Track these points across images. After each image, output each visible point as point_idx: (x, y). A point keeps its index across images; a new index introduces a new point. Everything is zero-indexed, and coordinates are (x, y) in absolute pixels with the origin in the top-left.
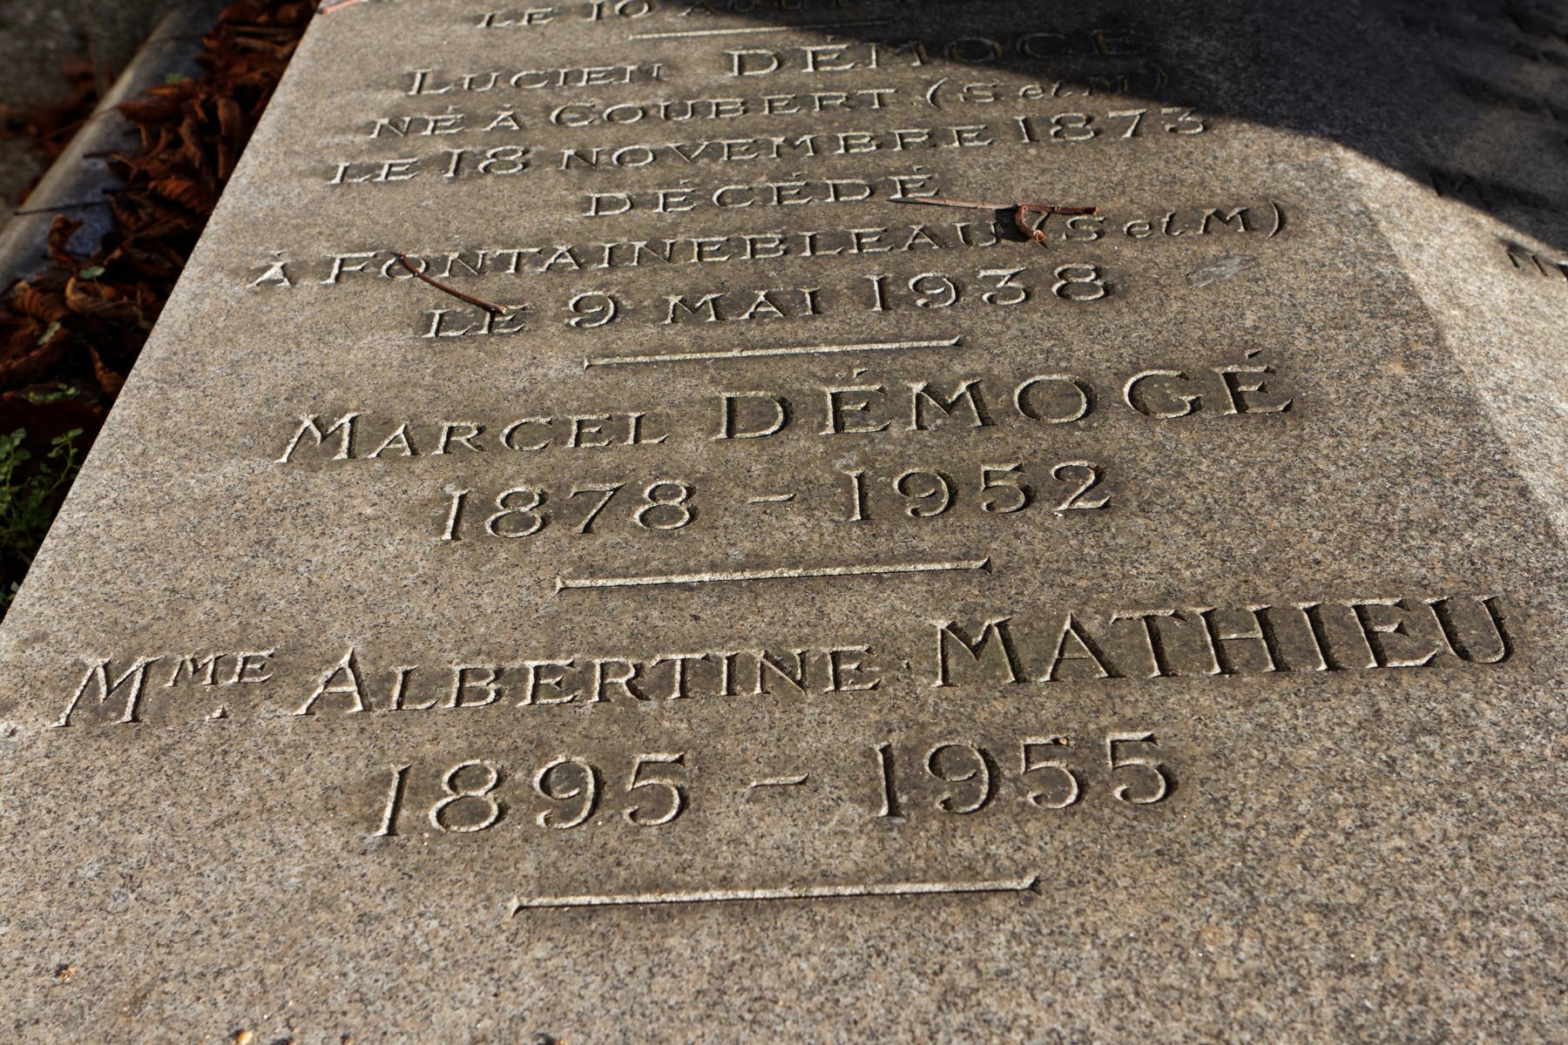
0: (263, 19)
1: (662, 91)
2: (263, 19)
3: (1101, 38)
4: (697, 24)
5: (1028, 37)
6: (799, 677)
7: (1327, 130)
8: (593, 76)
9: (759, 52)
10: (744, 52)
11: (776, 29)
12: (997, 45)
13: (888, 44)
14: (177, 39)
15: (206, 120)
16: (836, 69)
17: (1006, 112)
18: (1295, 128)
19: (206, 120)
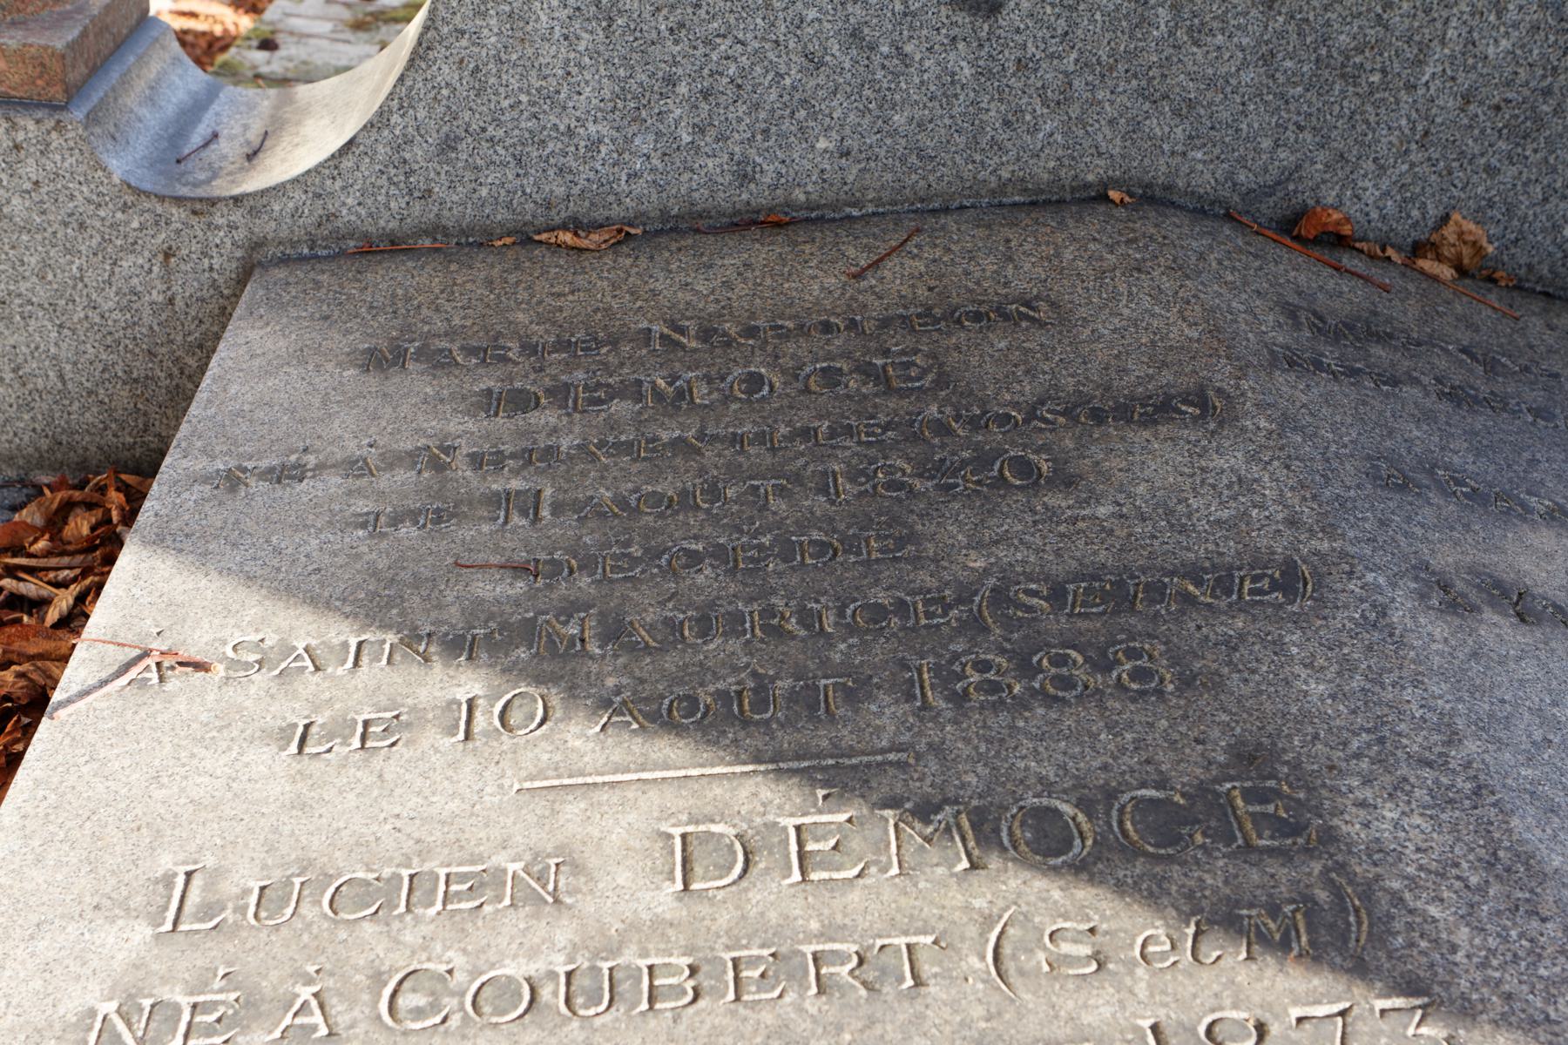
0: (42, 544)
1: (564, 934)
2: (42, 544)
3: (1240, 802)
4: (617, 756)
5: (1126, 797)
6: (140, 1034)
7: (1338, 960)
8: (454, 888)
9: (715, 828)
10: (690, 829)
11: (738, 769)
12: (1081, 817)
13: (913, 813)
14: (108, 458)
15: (47, 536)
16: (835, 875)
17: (1122, 1005)
18: (1348, 971)
19: (47, 536)
